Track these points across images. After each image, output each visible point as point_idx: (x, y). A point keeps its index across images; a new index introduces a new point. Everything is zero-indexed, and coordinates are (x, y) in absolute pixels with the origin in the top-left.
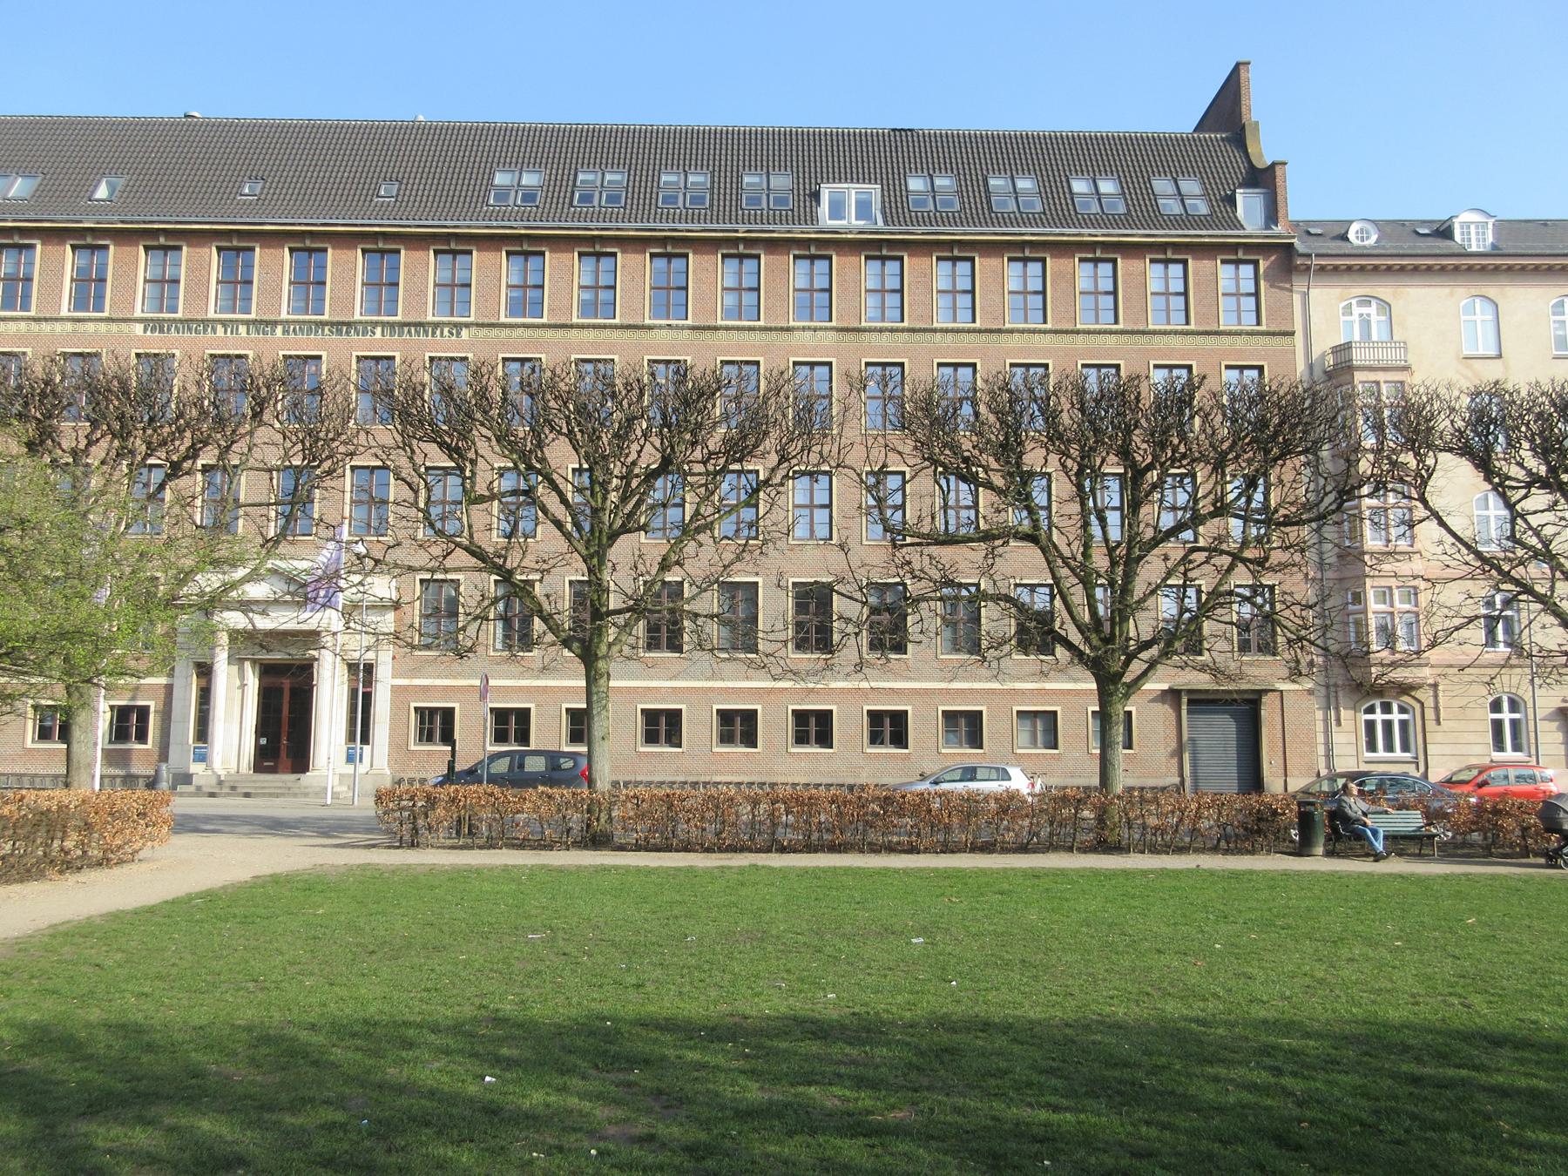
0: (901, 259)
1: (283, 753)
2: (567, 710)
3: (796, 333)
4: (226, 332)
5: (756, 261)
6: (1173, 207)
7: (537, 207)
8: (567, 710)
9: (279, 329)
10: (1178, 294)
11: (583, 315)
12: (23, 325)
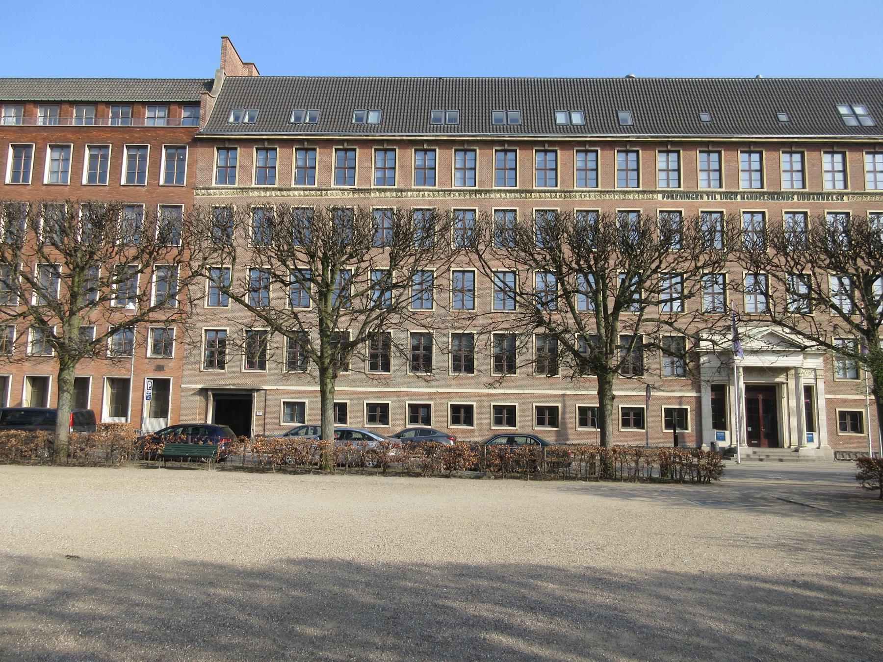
0: (556, 151)
1: (762, 436)
2: (367, 404)
3: (292, 192)
4: (708, 199)
5: (474, 153)
6: (853, 122)
7: (521, 125)
8: (367, 404)
9: (739, 197)
10: (756, 171)
11: (337, 183)
12: (231, 192)
